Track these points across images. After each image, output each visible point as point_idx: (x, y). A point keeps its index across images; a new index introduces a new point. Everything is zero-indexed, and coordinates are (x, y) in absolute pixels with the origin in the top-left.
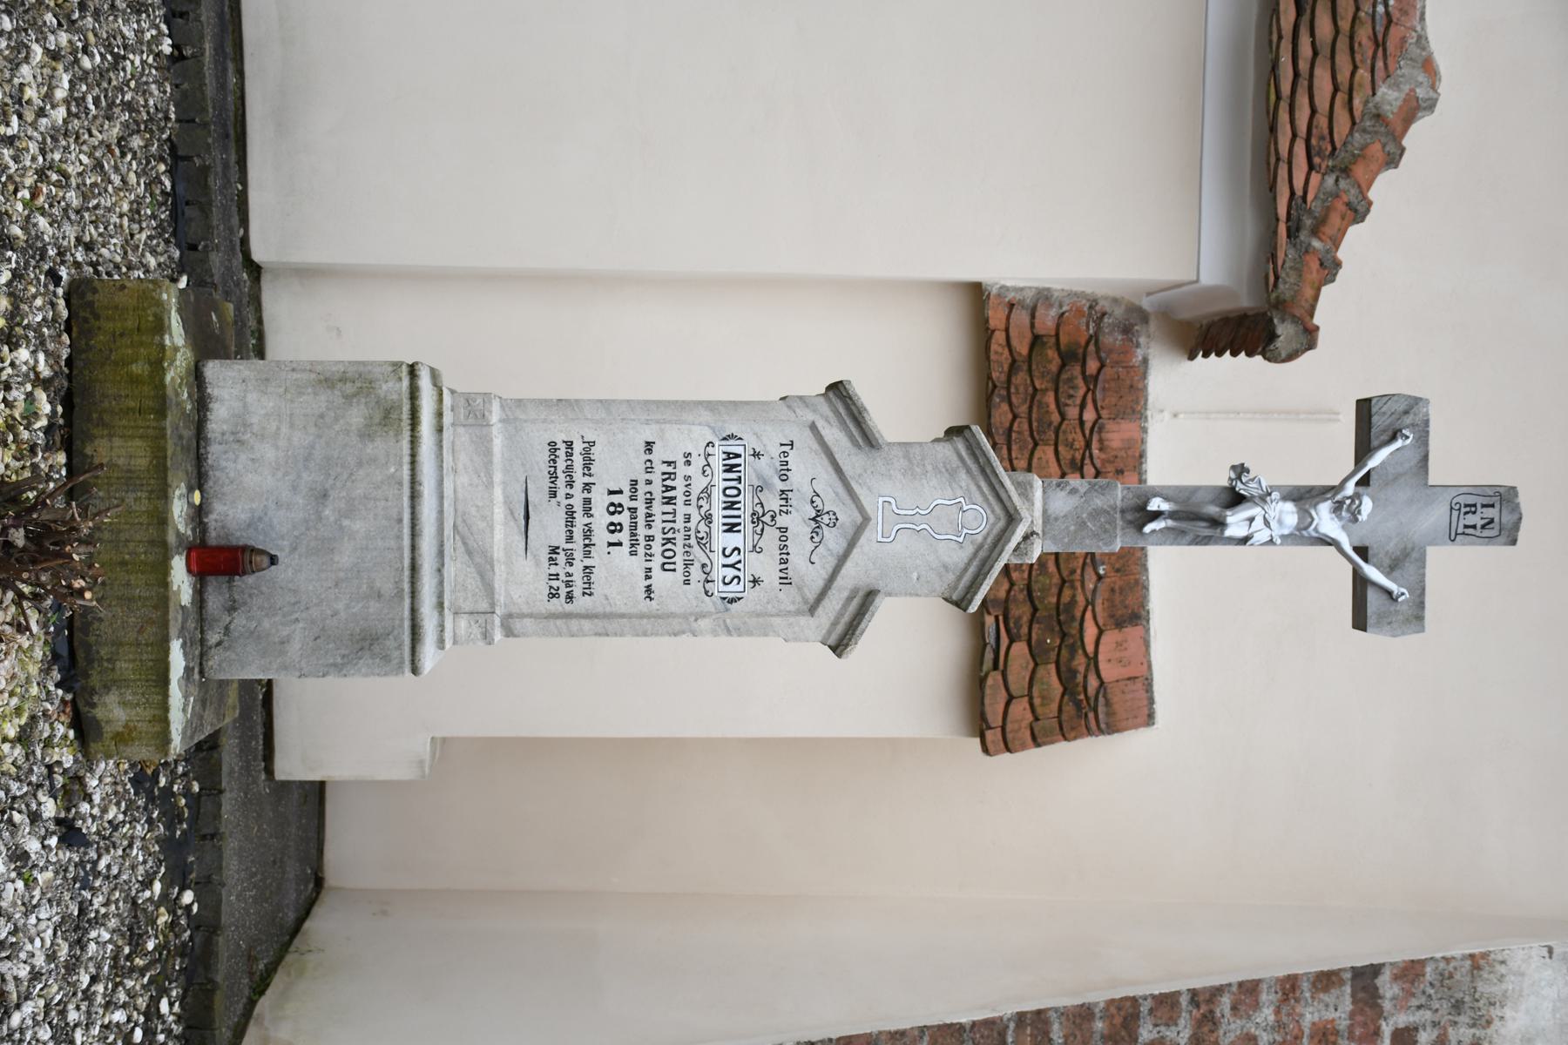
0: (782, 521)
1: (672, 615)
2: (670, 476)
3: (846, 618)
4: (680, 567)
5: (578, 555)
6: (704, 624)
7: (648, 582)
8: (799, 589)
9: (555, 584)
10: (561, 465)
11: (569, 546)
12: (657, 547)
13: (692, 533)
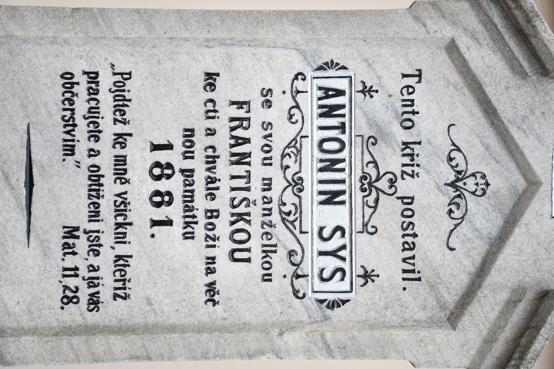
0: (405, 187)
1: (245, 327)
2: (241, 122)
3: (508, 333)
4: (256, 255)
5: (107, 239)
6: (292, 339)
7: (211, 278)
8: (432, 287)
9: (72, 282)
10: (81, 107)
11: (94, 226)
12: (223, 227)
13: (274, 206)
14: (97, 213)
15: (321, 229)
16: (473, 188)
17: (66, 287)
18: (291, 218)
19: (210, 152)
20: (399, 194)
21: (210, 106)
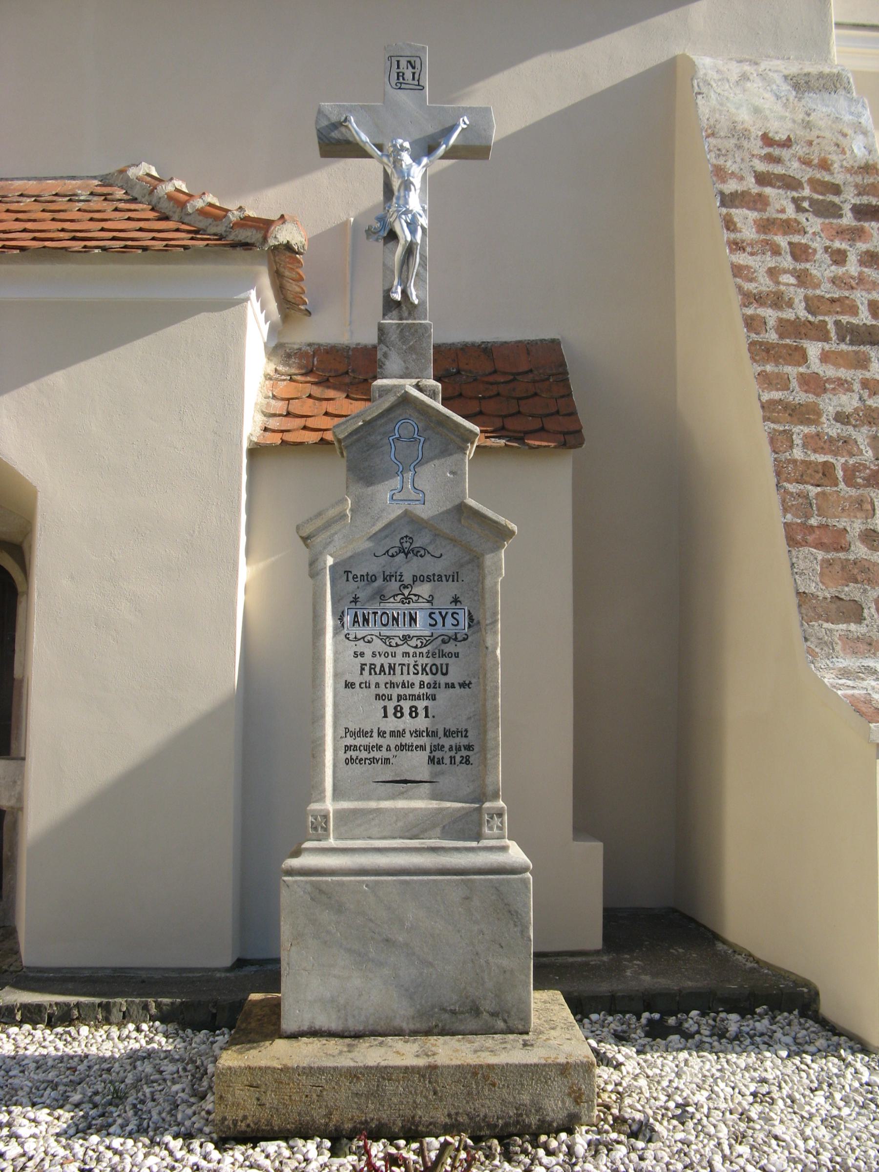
0: (408, 580)
2: (372, 667)
4: (444, 660)
5: (436, 741)
8: (462, 566)
9: (458, 759)
10: (364, 755)
13: (418, 651)
14: (421, 746)
15: (430, 625)
16: (408, 544)
17: (461, 763)
18: (425, 642)
19: (388, 686)
20: (411, 583)
21: (363, 685)
